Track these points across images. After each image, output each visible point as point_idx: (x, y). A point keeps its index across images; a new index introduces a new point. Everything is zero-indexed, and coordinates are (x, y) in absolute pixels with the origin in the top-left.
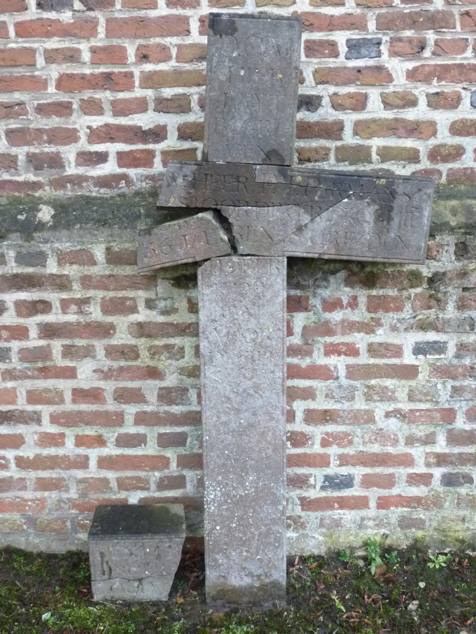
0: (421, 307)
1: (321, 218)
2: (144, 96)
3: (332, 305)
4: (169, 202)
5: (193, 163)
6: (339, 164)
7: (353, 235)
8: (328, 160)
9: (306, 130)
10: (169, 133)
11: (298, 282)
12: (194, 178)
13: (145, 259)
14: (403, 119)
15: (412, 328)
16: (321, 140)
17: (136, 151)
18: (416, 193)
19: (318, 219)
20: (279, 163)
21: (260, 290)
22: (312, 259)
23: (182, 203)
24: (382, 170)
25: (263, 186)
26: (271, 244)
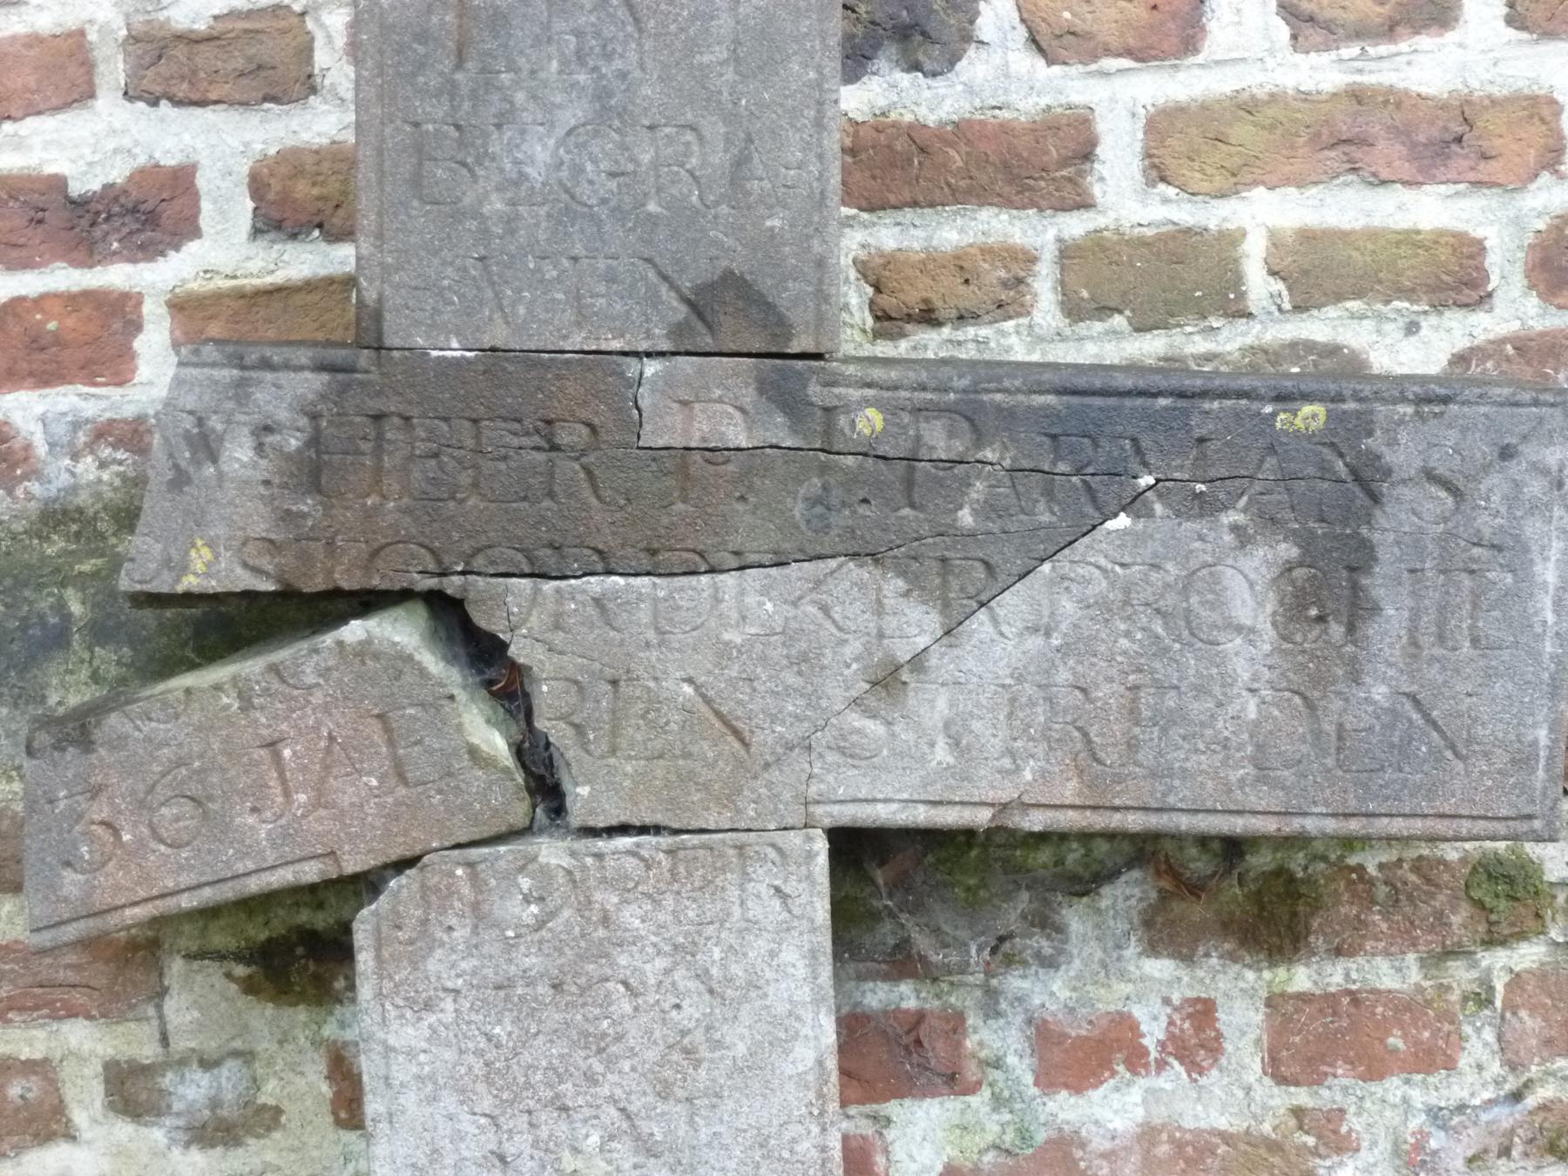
0: (1548, 1042)
1: (995, 621)
2: (72, 24)
3: (1084, 1055)
4: (184, 569)
5: (303, 356)
6: (1082, 328)
7: (1171, 701)
8: (1024, 311)
9: (895, 168)
10: (206, 206)
11: (904, 945)
12: (315, 441)
13: (69, 875)
14: (1391, 90)
15: (1505, 1152)
16: (985, 214)
17: (41, 301)
18: (1486, 468)
19: (980, 623)
20: (757, 346)
21: (691, 1012)
22: (965, 837)
23: (257, 571)
24: (1298, 348)
25: (683, 468)
26: (740, 763)
